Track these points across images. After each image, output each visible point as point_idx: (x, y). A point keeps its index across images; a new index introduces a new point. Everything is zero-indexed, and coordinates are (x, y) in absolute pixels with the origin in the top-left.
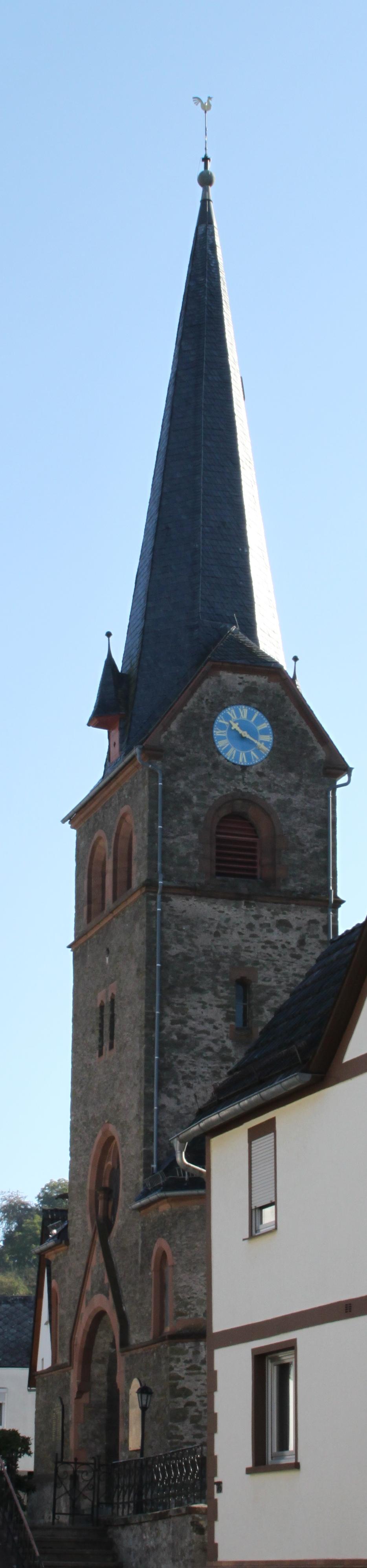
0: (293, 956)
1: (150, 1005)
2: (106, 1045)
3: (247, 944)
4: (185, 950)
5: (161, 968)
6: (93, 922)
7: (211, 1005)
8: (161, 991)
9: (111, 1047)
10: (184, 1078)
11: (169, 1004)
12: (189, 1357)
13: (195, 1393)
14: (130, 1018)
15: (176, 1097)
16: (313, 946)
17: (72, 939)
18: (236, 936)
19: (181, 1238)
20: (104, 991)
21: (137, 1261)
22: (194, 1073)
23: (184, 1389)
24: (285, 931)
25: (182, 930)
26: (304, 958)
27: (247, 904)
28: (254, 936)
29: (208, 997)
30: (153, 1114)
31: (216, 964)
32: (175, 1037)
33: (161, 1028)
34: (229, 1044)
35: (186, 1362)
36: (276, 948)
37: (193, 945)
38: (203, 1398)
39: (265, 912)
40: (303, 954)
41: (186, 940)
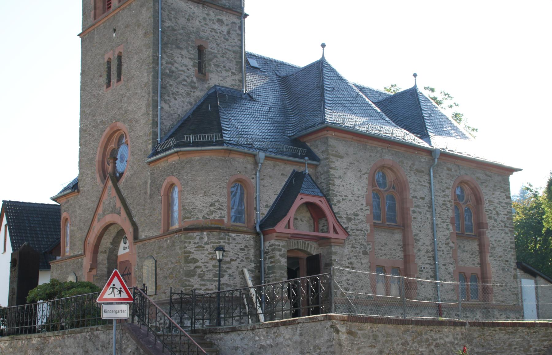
0: (225, 39)
1: (156, 51)
2: (114, 79)
3: (203, 28)
4: (173, 25)
5: (162, 32)
6: (97, 20)
7: (186, 57)
8: (162, 45)
9: (119, 80)
10: (172, 94)
11: (165, 53)
12: (197, 241)
13: (201, 261)
14: (137, 61)
15: (168, 104)
16: (234, 35)
17: (81, 31)
18: (198, 23)
19: (187, 175)
20: (112, 52)
21: (146, 193)
22: (178, 92)
23: (194, 259)
24: (221, 25)
25: (171, 13)
26: (230, 41)
27: (203, 7)
28: (206, 24)
29: (184, 52)
30: (157, 111)
31: (188, 35)
32: (168, 71)
33: (162, 65)
34: (195, 79)
35: (195, 243)
36: (217, 33)
37: (176, 22)
38: (205, 264)
39: (211, 13)
40: (229, 38)
41: (173, 20)
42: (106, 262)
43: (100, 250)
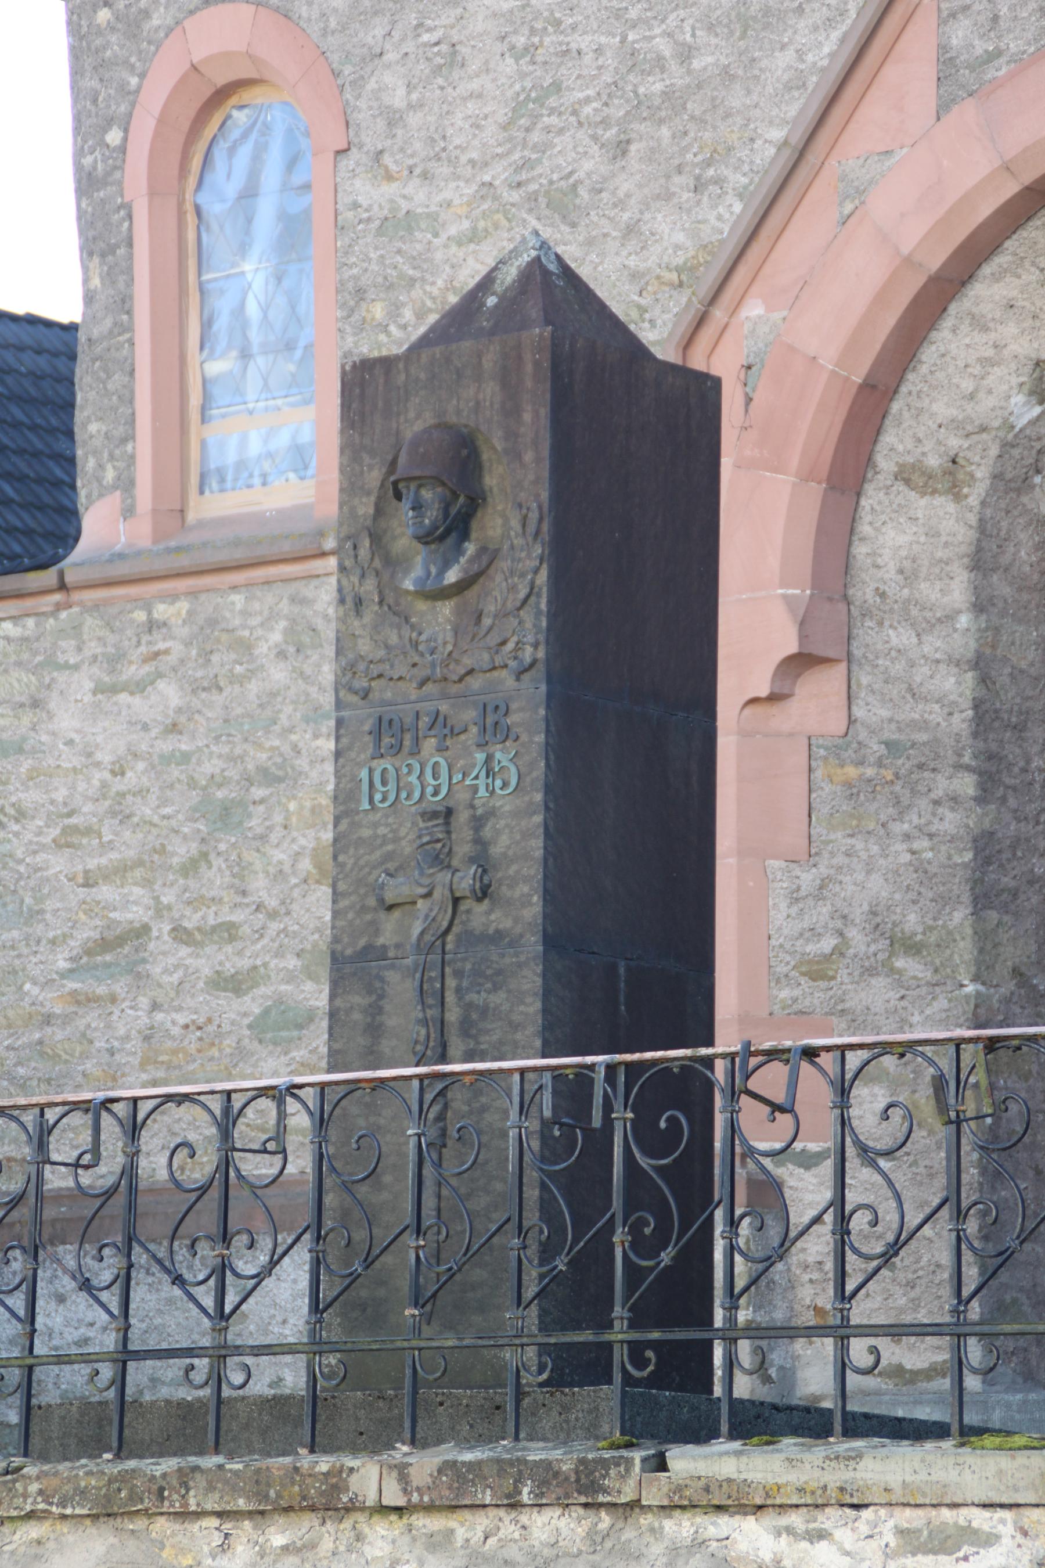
42: (956, 591)
43: (894, 445)
